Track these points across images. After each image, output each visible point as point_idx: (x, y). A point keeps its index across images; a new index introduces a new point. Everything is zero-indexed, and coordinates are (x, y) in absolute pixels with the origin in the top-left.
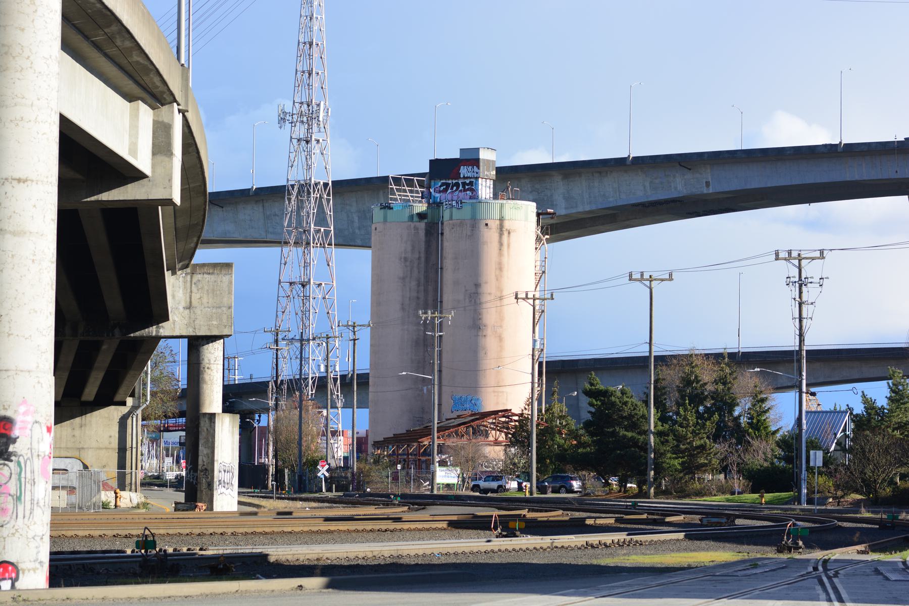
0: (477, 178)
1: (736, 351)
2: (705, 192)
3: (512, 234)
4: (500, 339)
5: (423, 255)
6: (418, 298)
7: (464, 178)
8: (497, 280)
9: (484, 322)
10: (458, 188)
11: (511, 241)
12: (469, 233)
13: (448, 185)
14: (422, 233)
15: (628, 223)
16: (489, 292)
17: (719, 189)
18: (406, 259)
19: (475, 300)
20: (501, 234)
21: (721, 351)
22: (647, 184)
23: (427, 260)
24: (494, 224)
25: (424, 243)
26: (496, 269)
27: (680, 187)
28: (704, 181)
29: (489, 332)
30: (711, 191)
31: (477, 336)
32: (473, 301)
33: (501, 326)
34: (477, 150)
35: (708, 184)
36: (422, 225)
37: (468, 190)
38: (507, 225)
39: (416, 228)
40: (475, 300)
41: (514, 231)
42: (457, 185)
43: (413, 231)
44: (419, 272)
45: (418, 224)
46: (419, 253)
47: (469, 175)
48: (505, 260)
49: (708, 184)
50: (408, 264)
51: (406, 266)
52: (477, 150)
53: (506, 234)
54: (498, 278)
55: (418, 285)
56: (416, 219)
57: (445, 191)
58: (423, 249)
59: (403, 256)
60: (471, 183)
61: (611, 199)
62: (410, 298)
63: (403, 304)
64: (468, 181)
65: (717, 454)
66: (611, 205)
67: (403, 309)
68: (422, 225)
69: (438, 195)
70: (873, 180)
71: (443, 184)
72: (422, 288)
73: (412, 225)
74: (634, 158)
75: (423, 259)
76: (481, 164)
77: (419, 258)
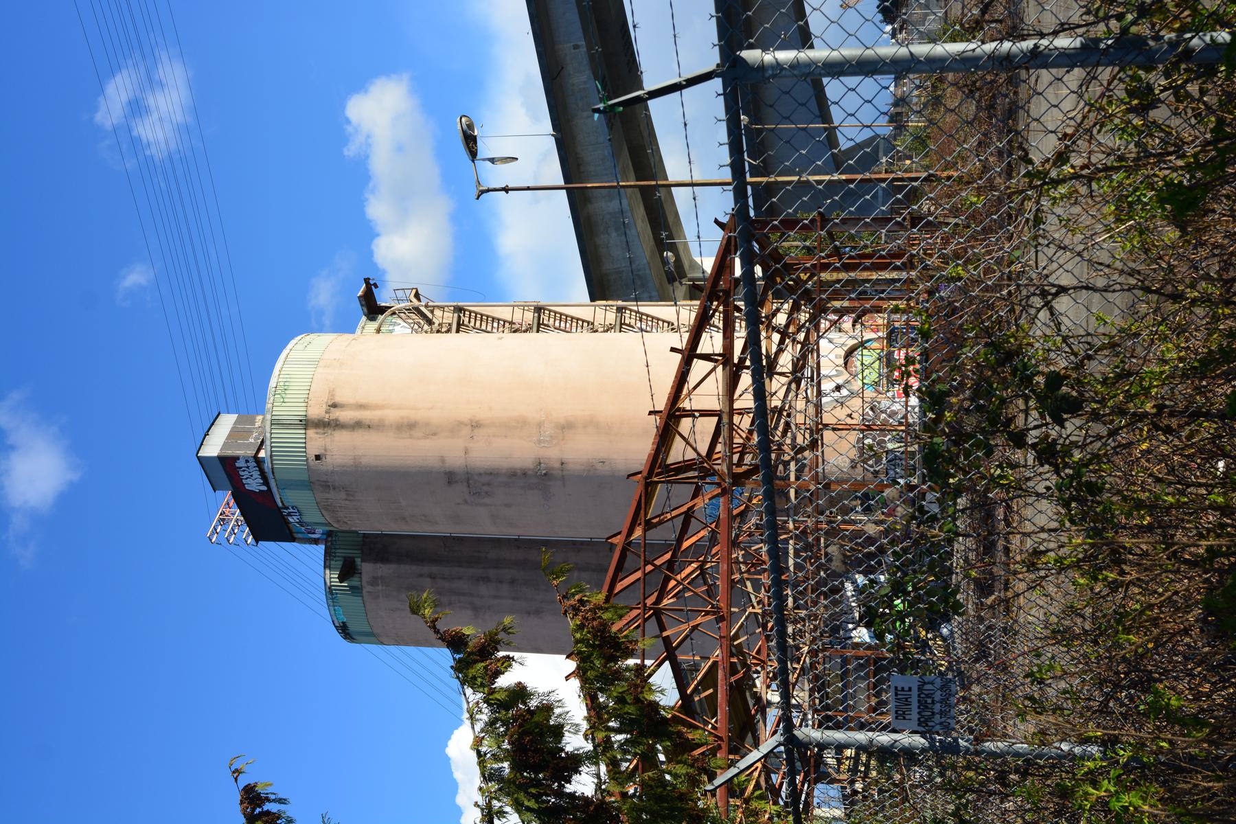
2: (585, 49)
3: (338, 399)
4: (567, 427)
5: (426, 569)
6: (513, 582)
8: (435, 434)
9: (532, 467)
11: (352, 401)
12: (343, 495)
14: (384, 569)
15: (646, 134)
16: (462, 454)
17: (580, 34)
19: (484, 485)
20: (335, 425)
23: (435, 560)
24: (316, 442)
25: (402, 566)
26: (411, 437)
28: (573, 51)
29: (553, 454)
30: (583, 43)
31: (563, 478)
32: (485, 488)
33: (540, 425)
35: (576, 47)
36: (367, 569)
38: (317, 412)
39: (374, 581)
40: (484, 485)
41: (332, 393)
43: (380, 588)
44: (460, 578)
45: (365, 578)
46: (421, 576)
47: (256, 474)
48: (391, 415)
49: (576, 47)
50: (445, 599)
51: (450, 604)
53: (337, 414)
54: (432, 431)
55: (486, 580)
56: (355, 582)
58: (414, 568)
61: (606, 152)
62: (514, 598)
63: (528, 613)
65: (802, 720)
67: (538, 612)
68: (367, 569)
72: (492, 573)
73: (367, 589)
74: (554, 130)
75: (435, 569)
76: (229, 453)
77: (432, 577)
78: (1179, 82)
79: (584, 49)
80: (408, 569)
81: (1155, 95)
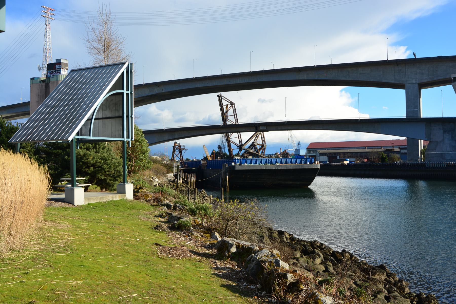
0: (61, 69)
1: (220, 125)
7: (57, 69)
10: (55, 72)
13: (52, 71)
14: (44, 87)
17: (166, 91)
18: (39, 95)
21: (254, 123)
22: (149, 91)
27: (156, 91)
34: (60, 59)
35: (163, 90)
36: (44, 84)
37: (58, 72)
39: (42, 85)
42: (55, 71)
45: (42, 84)
46: (43, 93)
47: (58, 68)
49: (163, 90)
50: (39, 97)
51: (39, 98)
52: (60, 59)
56: (41, 82)
57: (52, 73)
59: (38, 94)
60: (59, 70)
64: (58, 70)
66: (141, 96)
68: (44, 84)
69: (50, 75)
70: (204, 87)
71: (51, 71)
73: (41, 84)
74: (145, 84)
75: (44, 95)
76: (62, 64)
77: (43, 95)
78: (454, 190)
79: (162, 92)
80: (44, 91)
81: (255, 296)
